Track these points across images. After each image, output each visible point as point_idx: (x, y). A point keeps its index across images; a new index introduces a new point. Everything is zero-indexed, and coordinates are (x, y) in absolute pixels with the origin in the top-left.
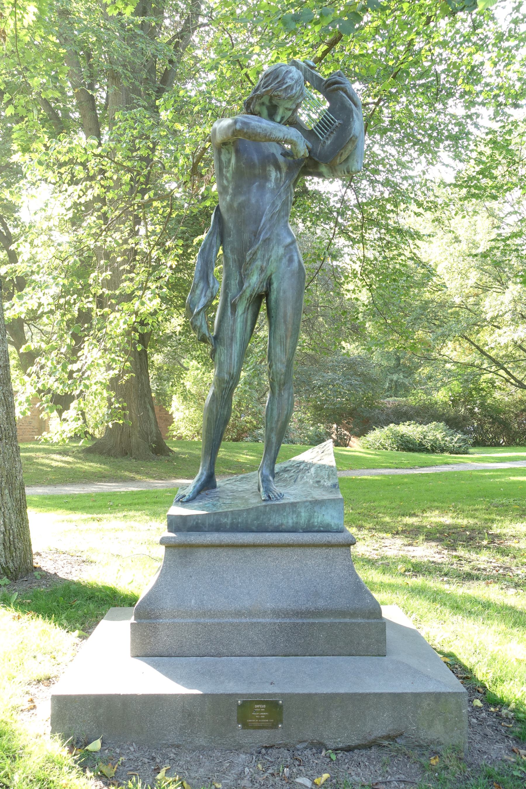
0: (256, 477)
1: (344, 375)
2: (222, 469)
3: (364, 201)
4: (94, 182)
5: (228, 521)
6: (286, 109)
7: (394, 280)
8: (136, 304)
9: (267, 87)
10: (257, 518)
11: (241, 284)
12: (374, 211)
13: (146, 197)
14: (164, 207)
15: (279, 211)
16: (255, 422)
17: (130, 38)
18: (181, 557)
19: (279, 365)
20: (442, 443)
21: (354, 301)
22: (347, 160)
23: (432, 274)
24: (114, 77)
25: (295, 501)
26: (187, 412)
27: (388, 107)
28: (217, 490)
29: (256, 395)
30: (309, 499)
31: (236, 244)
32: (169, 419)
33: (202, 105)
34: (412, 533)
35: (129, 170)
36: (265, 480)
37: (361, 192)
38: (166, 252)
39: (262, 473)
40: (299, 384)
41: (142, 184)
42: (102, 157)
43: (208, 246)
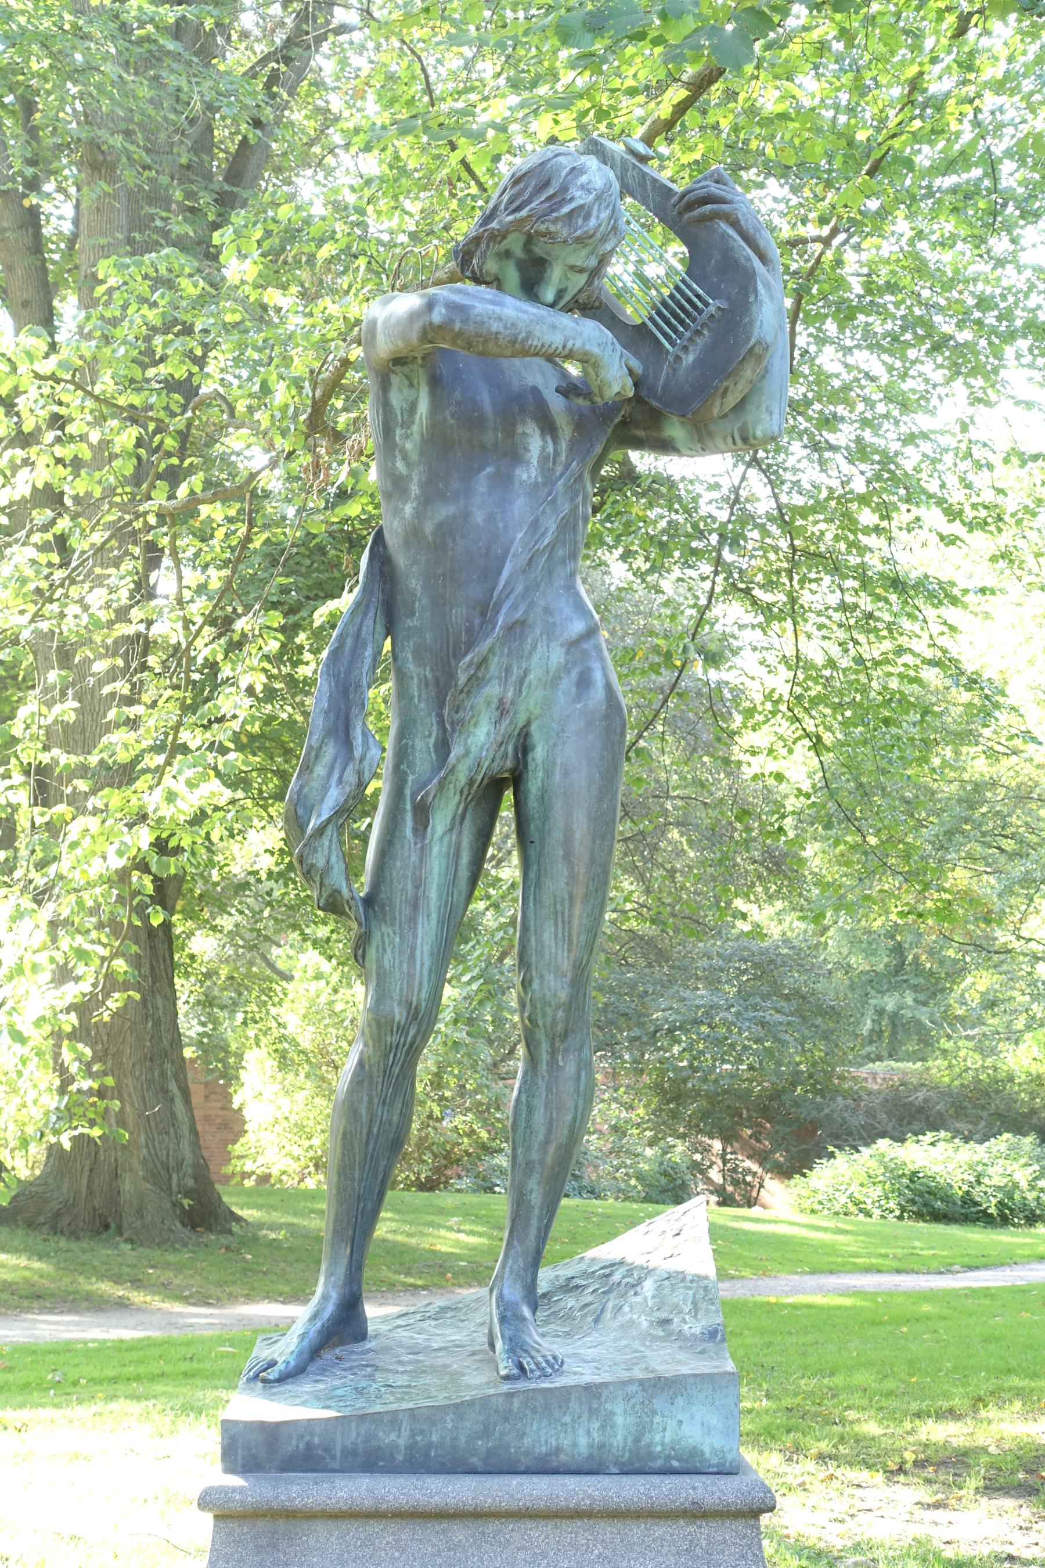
0: (481, 1304)
1: (743, 994)
2: (385, 1273)
3: (799, 501)
4: (34, 450)
5: (399, 1439)
6: (572, 268)
7: (887, 722)
8: (147, 795)
9: (518, 209)
10: (486, 1432)
11: (443, 747)
12: (825, 531)
13: (182, 491)
14: (230, 520)
15: (552, 545)
16: (484, 1135)
17: (146, 60)
18: (259, 1549)
19: (550, 978)
20: (1031, 1196)
21: (771, 782)
22: (741, 406)
23: (997, 706)
24: (98, 163)
25: (598, 1379)
26: (285, 1102)
27: (857, 248)
28: (369, 1345)
29: (487, 1054)
30: (638, 1373)
31: (429, 637)
32: (232, 1125)
33: (343, 243)
34: (948, 1465)
35: (134, 416)
36: (509, 1316)
37: (788, 476)
38: (236, 646)
39: (501, 1297)
40: (611, 1023)
41: (169, 455)
42: (58, 381)
43: (349, 642)
